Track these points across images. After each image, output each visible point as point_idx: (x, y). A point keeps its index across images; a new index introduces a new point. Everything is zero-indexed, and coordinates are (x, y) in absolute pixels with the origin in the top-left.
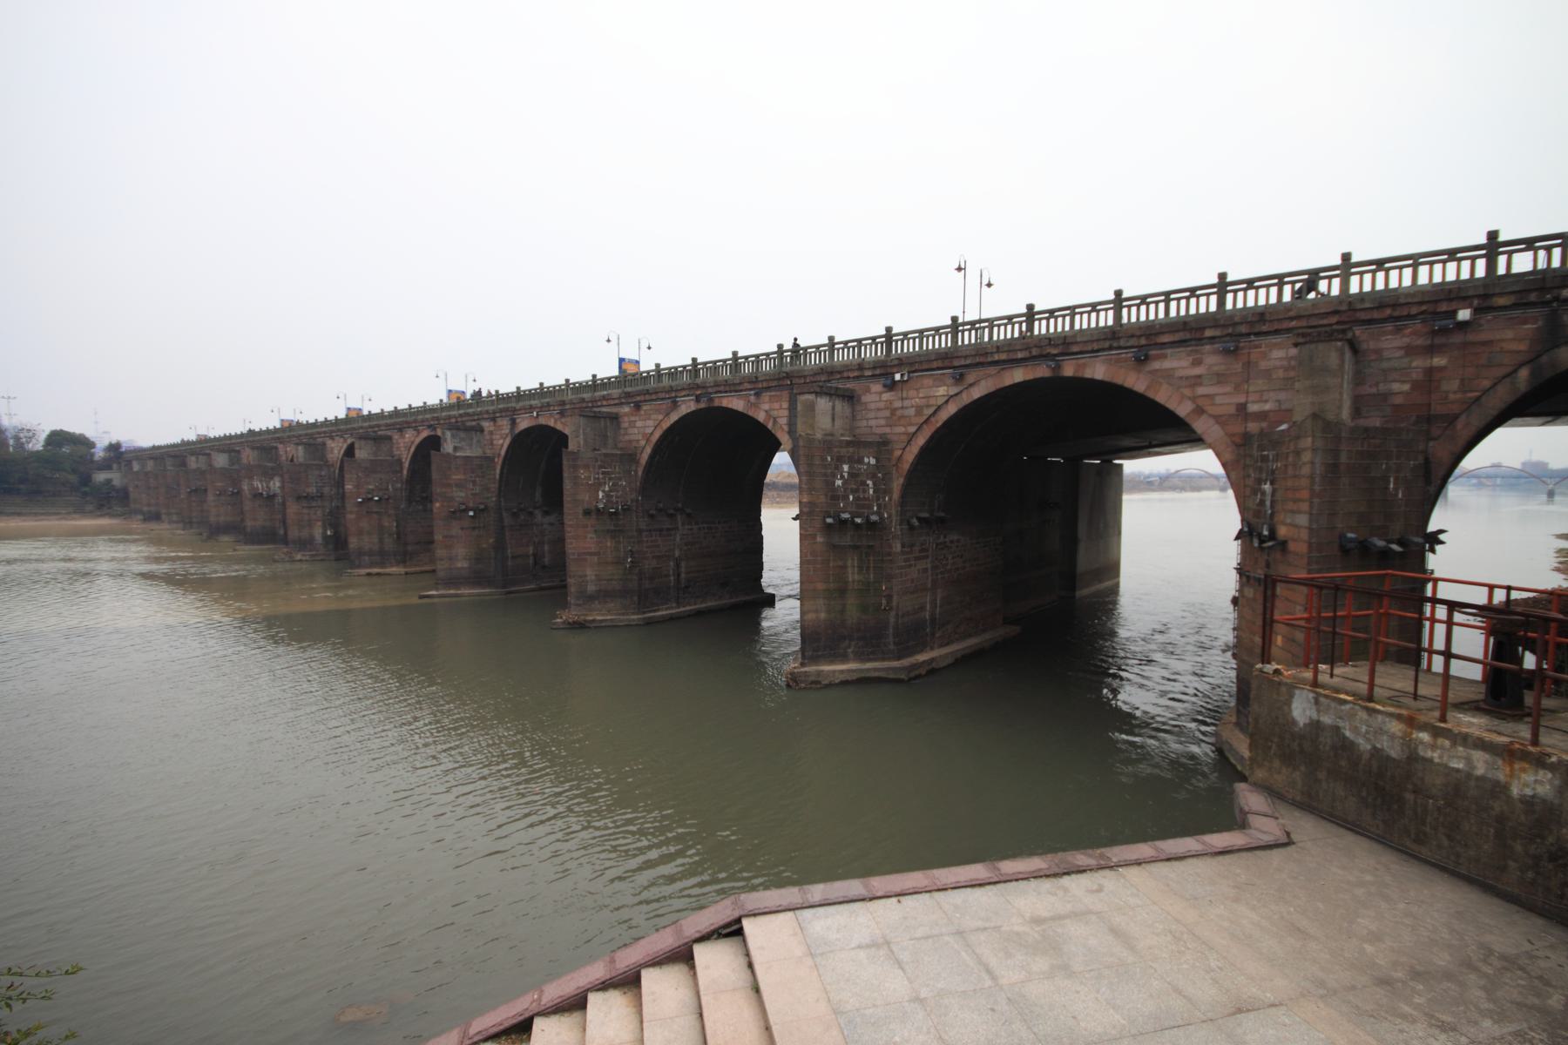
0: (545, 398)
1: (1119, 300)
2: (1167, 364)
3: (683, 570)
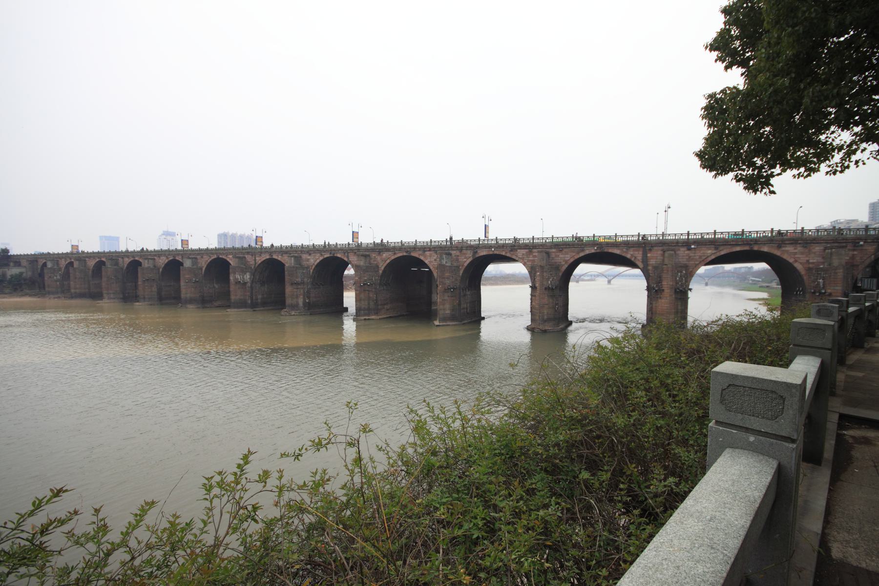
1: (715, 233)
2: (787, 249)
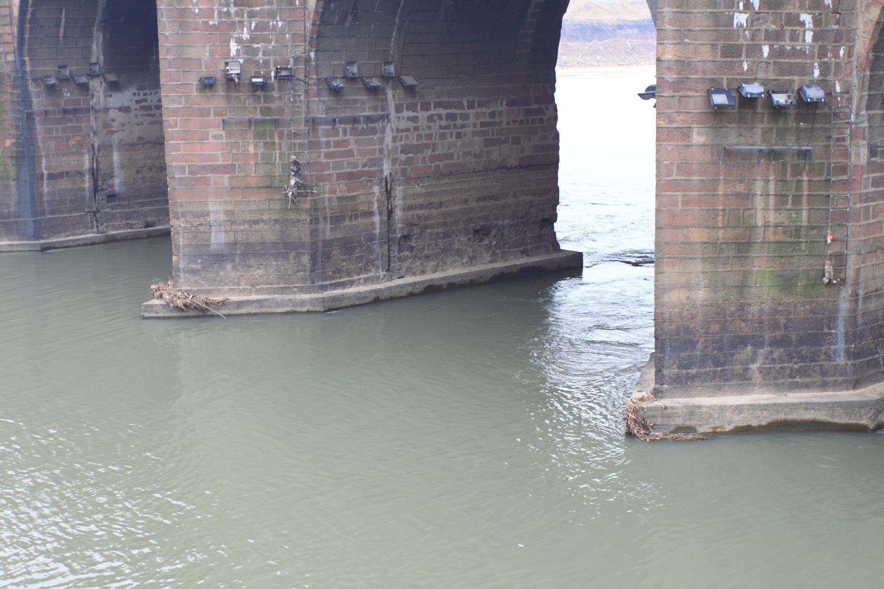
3: (398, 202)
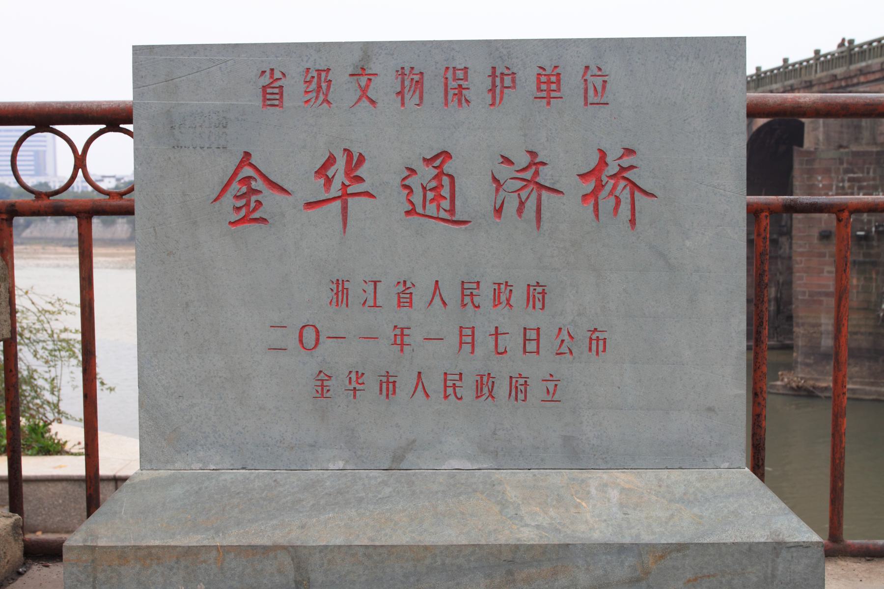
0: (790, 79)
